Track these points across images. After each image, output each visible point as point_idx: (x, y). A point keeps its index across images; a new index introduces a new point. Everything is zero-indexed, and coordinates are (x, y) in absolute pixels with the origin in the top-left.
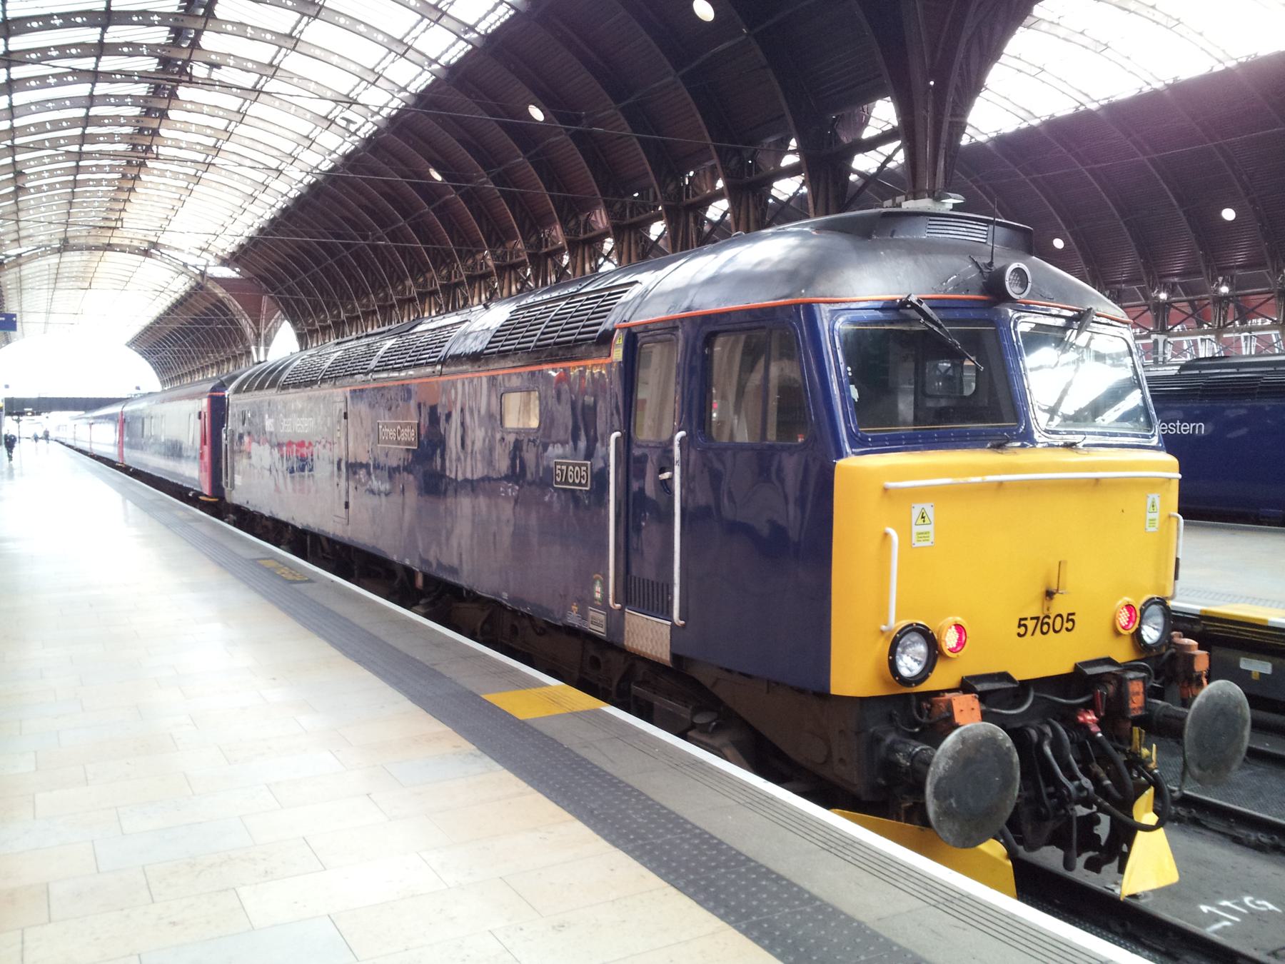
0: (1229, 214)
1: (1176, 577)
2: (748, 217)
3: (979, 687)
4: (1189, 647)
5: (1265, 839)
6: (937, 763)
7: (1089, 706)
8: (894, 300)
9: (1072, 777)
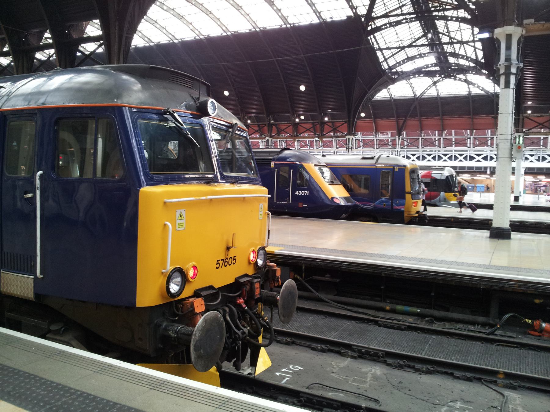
0: (302, 88)
1: (268, 238)
2: (23, 67)
3: (203, 293)
4: (273, 266)
5: (324, 347)
6: (196, 334)
7: (239, 296)
8: (161, 110)
9: (239, 329)
